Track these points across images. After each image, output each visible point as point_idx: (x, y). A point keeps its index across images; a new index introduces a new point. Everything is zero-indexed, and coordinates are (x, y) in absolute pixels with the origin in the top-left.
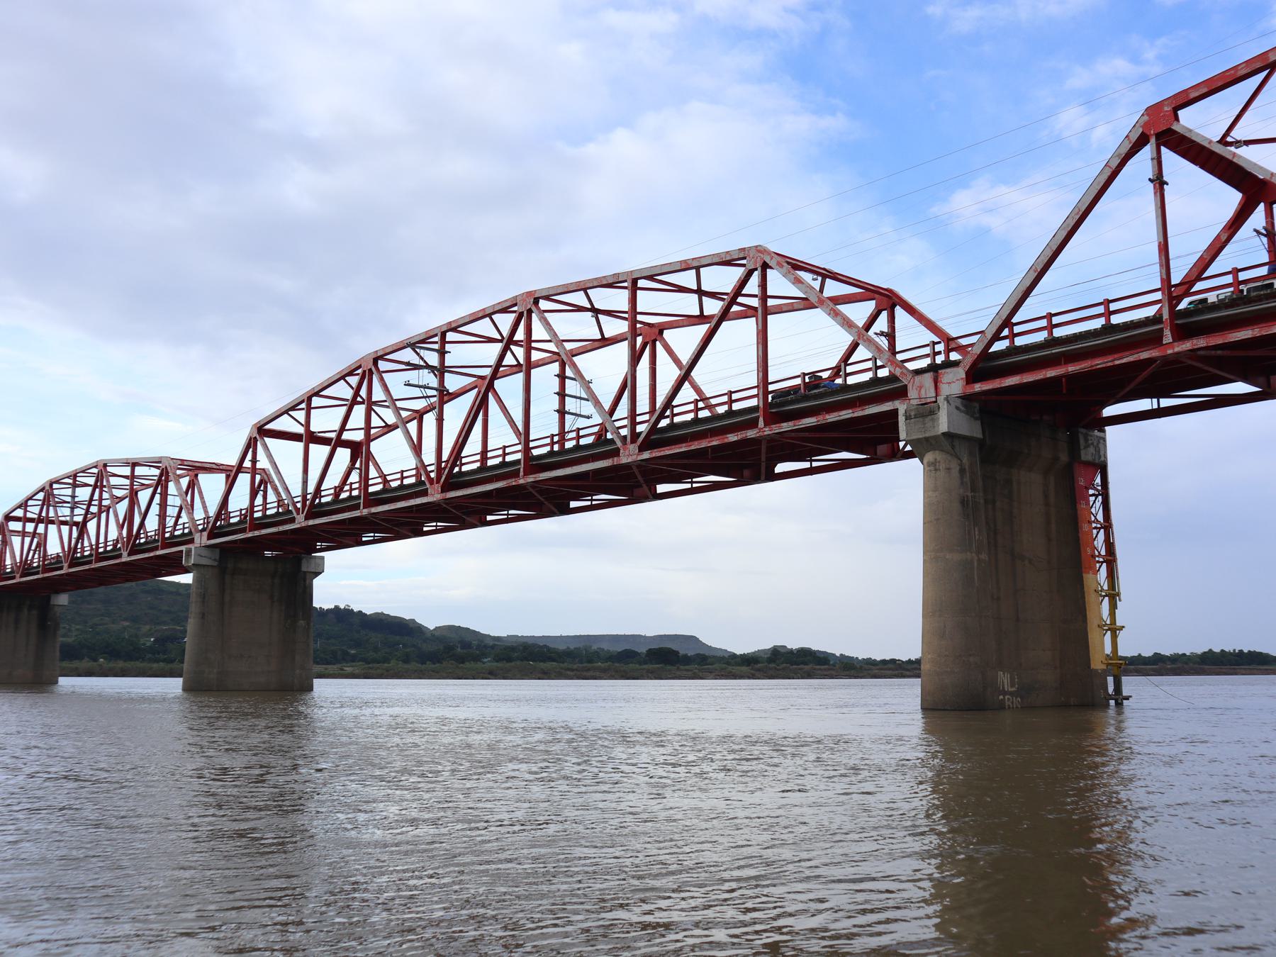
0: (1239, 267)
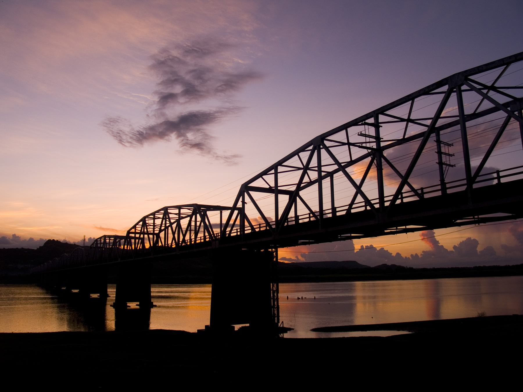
0: (424, 187)
